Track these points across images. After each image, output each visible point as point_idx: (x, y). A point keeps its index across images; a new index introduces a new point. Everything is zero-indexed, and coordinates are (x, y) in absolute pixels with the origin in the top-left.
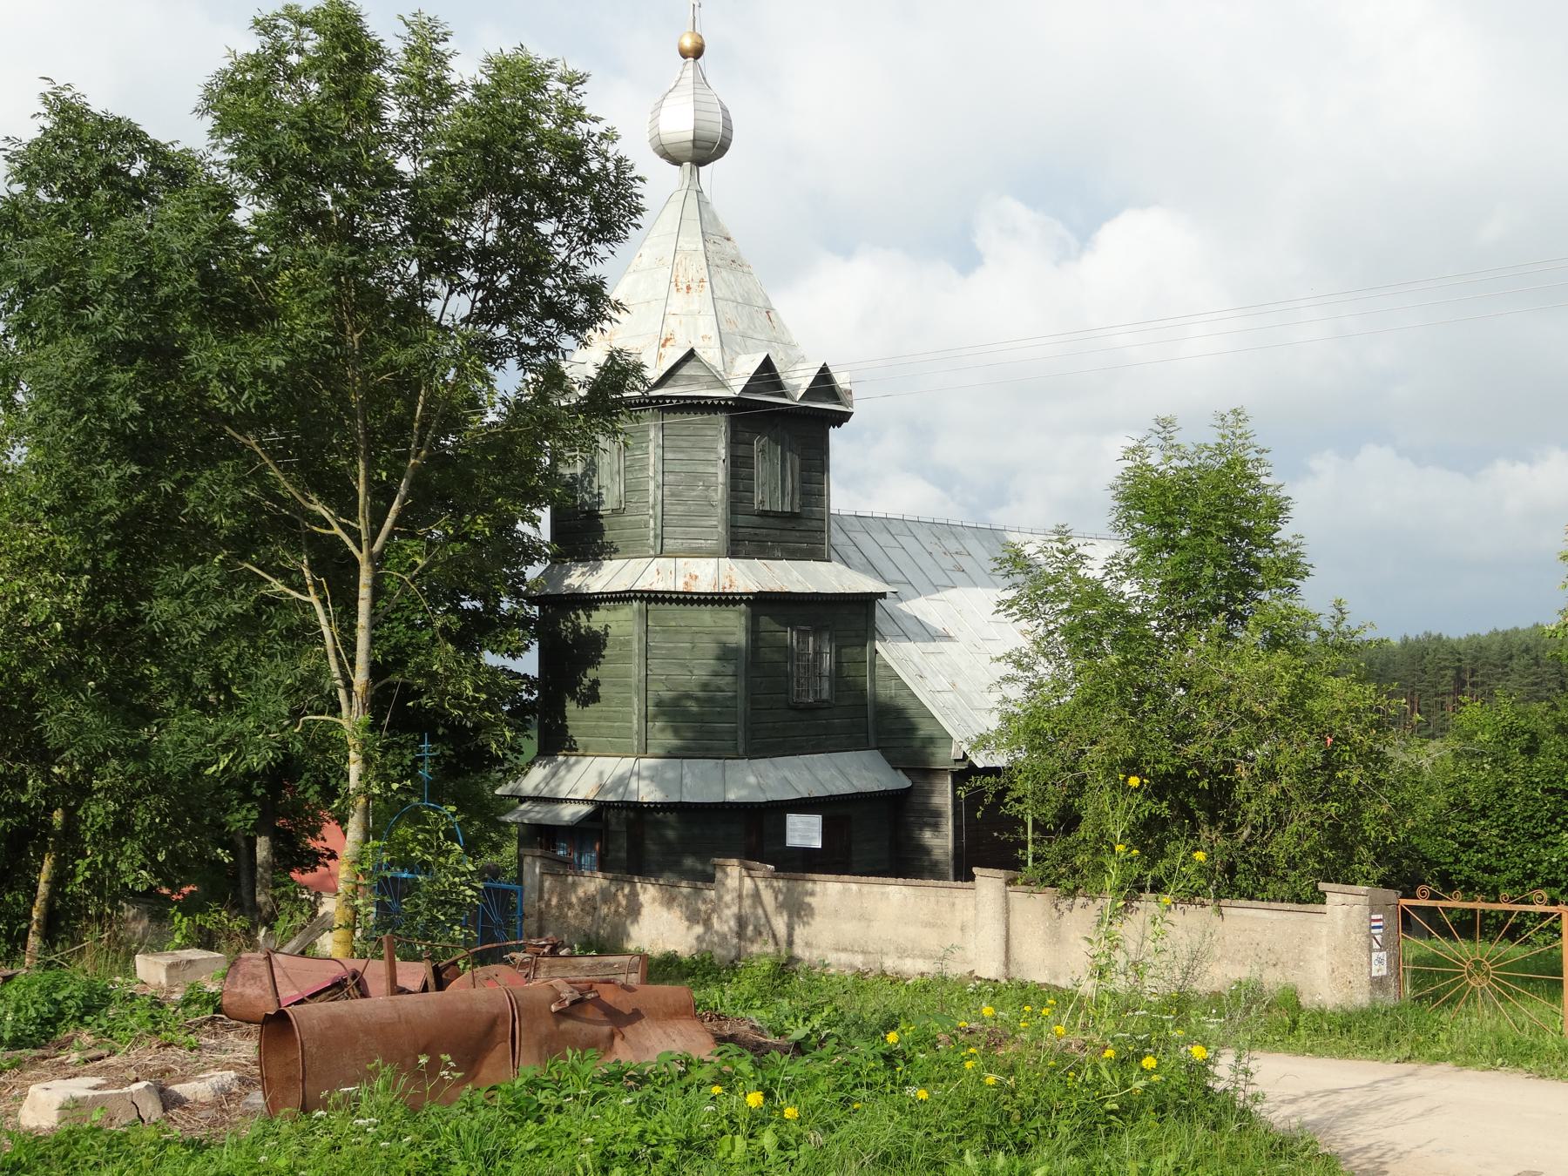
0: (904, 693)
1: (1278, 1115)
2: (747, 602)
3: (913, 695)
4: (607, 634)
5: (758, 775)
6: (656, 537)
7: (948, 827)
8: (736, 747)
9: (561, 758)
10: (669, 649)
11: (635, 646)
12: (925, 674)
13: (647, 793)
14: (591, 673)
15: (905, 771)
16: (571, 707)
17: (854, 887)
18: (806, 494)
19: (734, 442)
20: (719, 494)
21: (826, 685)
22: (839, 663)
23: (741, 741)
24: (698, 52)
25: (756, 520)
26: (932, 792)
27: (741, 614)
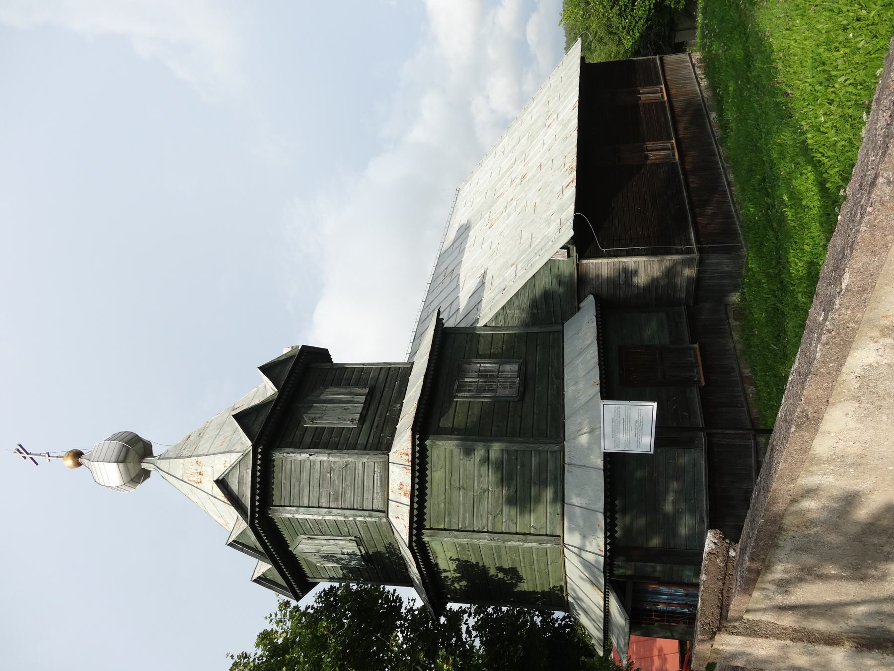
0: (516, 303)
1: (543, 495)
2: (422, 440)
3: (517, 294)
4: (458, 560)
5: (579, 433)
6: (370, 516)
7: (630, 261)
8: (553, 452)
9: (570, 599)
10: (465, 511)
11: (464, 541)
12: (503, 287)
13: (597, 545)
14: (492, 572)
15: (580, 300)
16: (524, 587)
17: (863, 356)
18: (358, 384)
19: (299, 446)
20: (337, 459)
21: (508, 367)
22: (491, 356)
23: (547, 447)
24: (77, 455)
25: (367, 425)
26: (598, 276)
27: (434, 444)
